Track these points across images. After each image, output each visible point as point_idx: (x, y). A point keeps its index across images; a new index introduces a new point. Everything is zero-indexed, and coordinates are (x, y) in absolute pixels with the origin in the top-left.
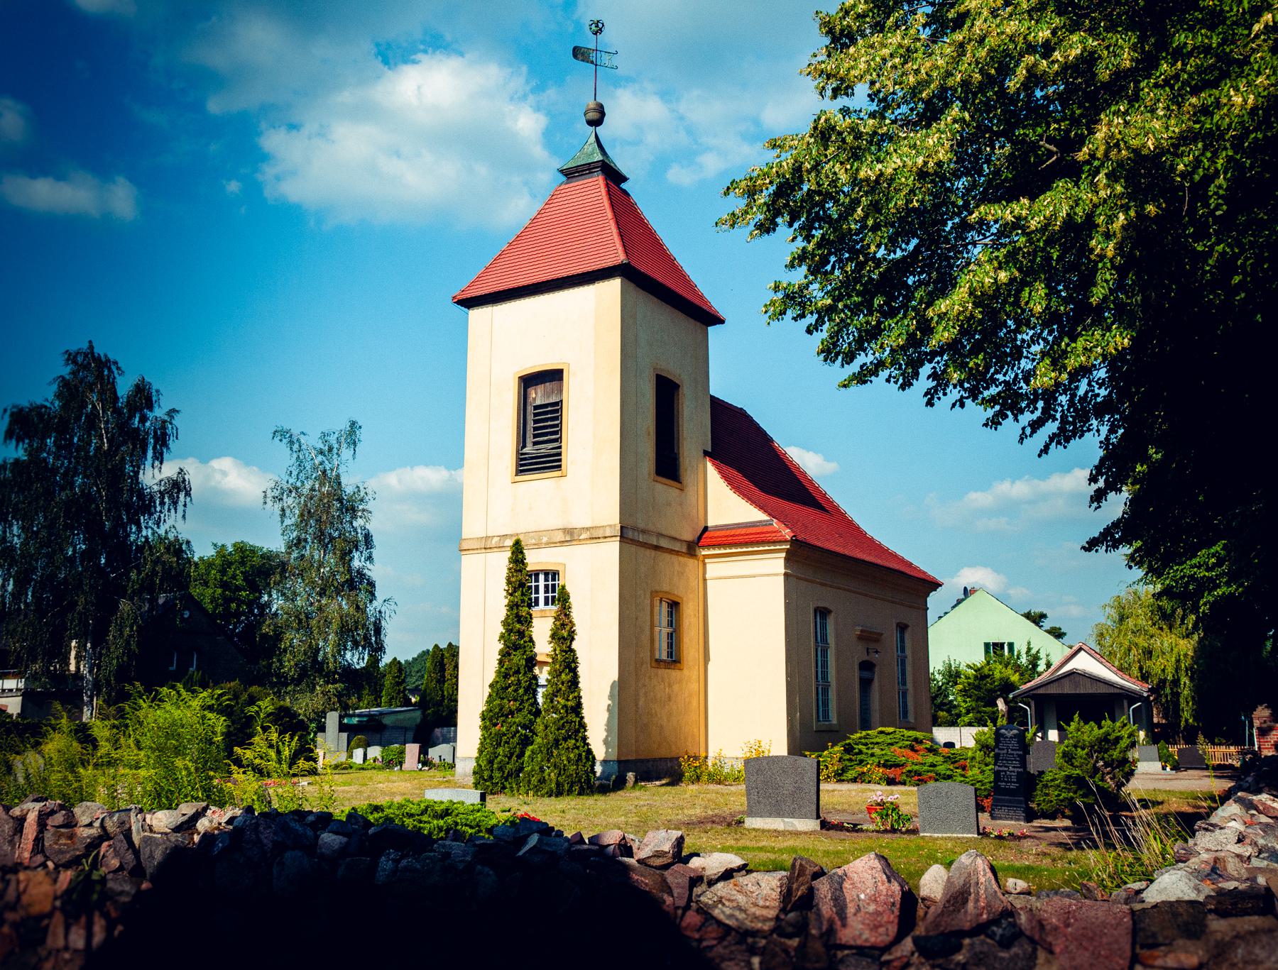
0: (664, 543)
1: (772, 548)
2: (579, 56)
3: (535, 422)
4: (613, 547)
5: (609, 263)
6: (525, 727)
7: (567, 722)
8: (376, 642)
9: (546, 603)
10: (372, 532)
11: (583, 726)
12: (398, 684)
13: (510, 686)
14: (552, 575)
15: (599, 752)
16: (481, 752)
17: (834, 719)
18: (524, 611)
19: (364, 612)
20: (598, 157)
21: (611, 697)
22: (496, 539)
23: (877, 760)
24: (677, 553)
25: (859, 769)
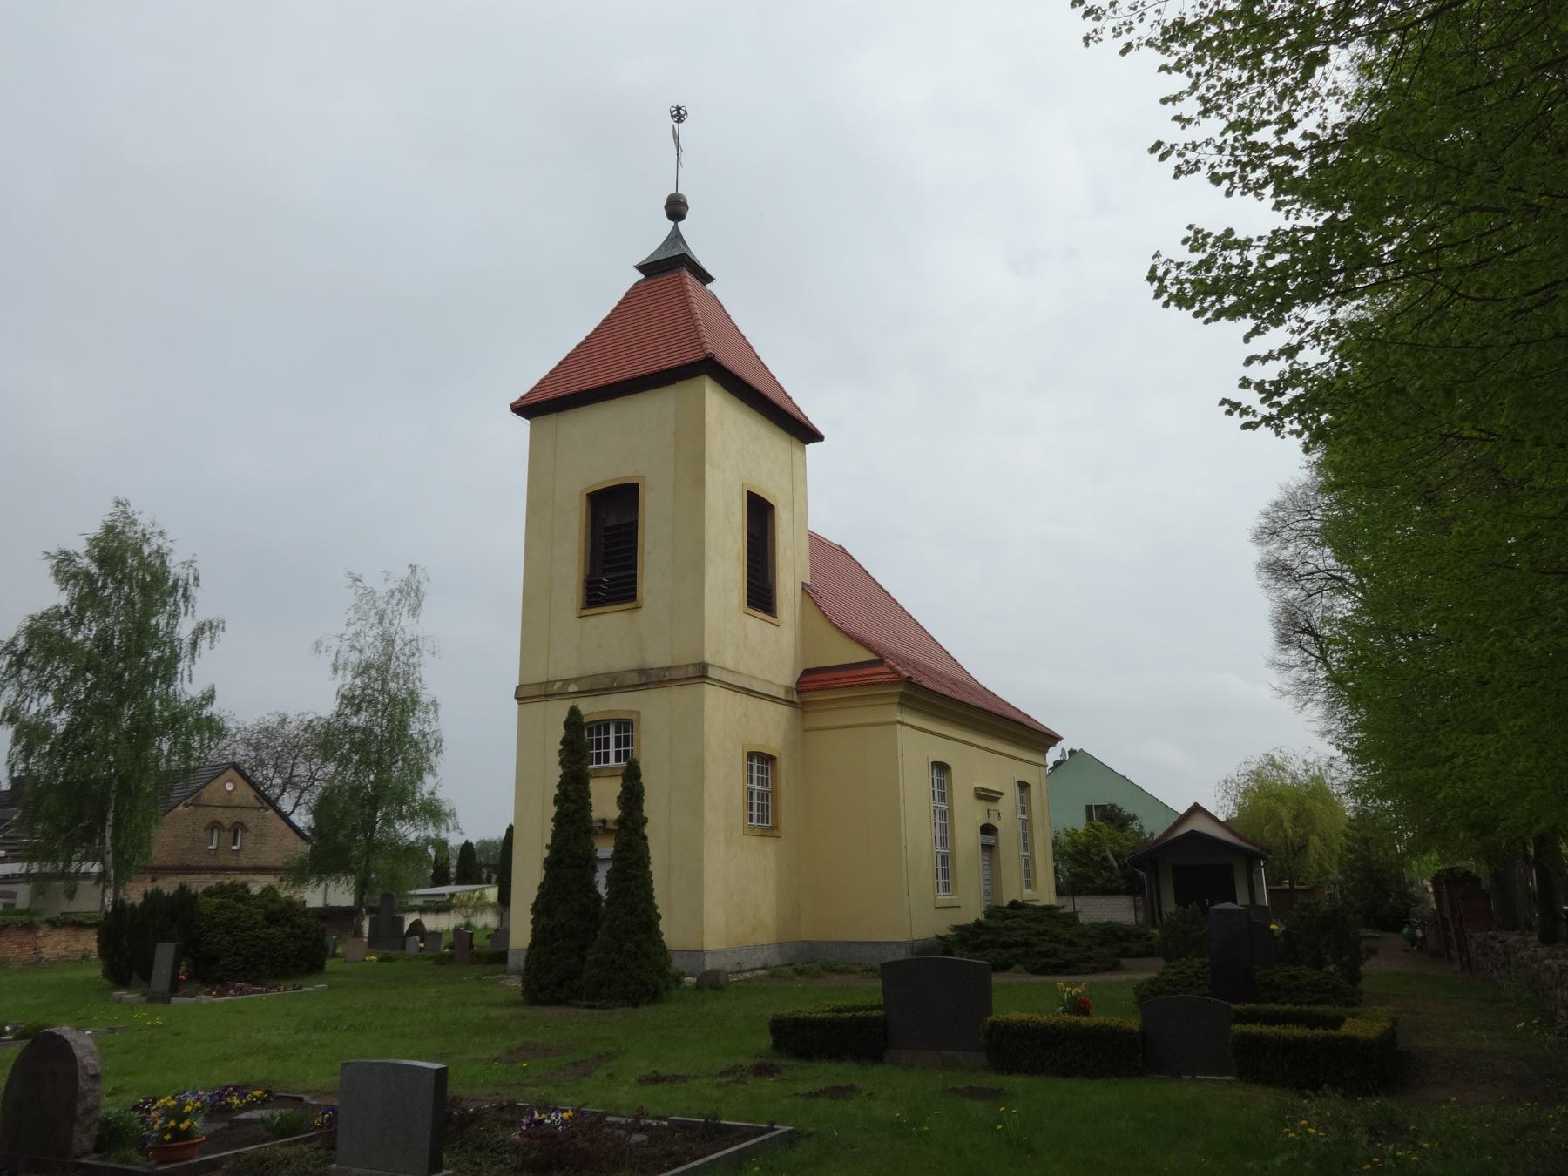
9: (618, 759)
22: (557, 685)
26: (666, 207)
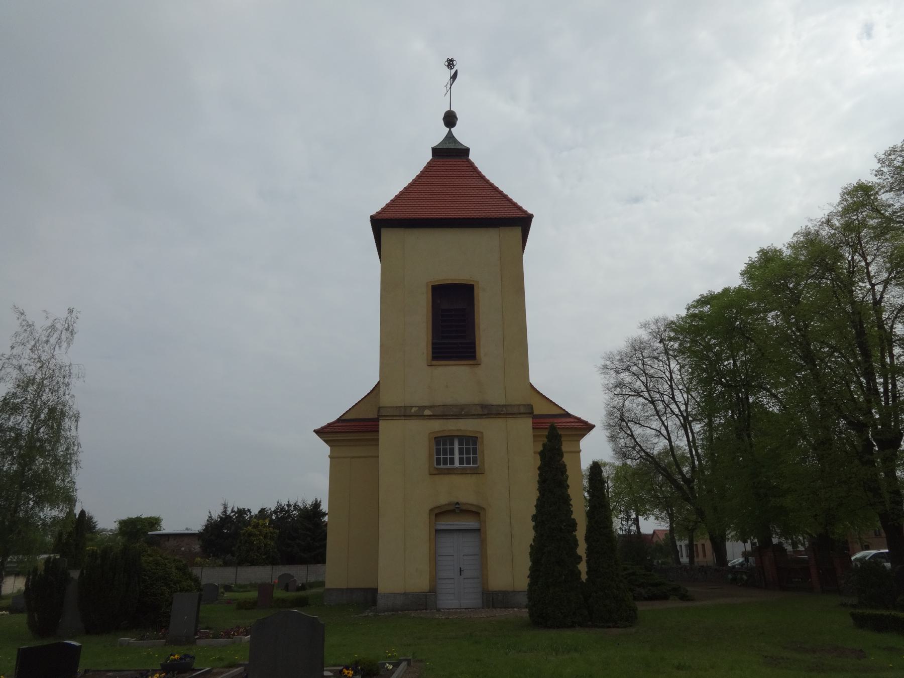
26: (444, 119)
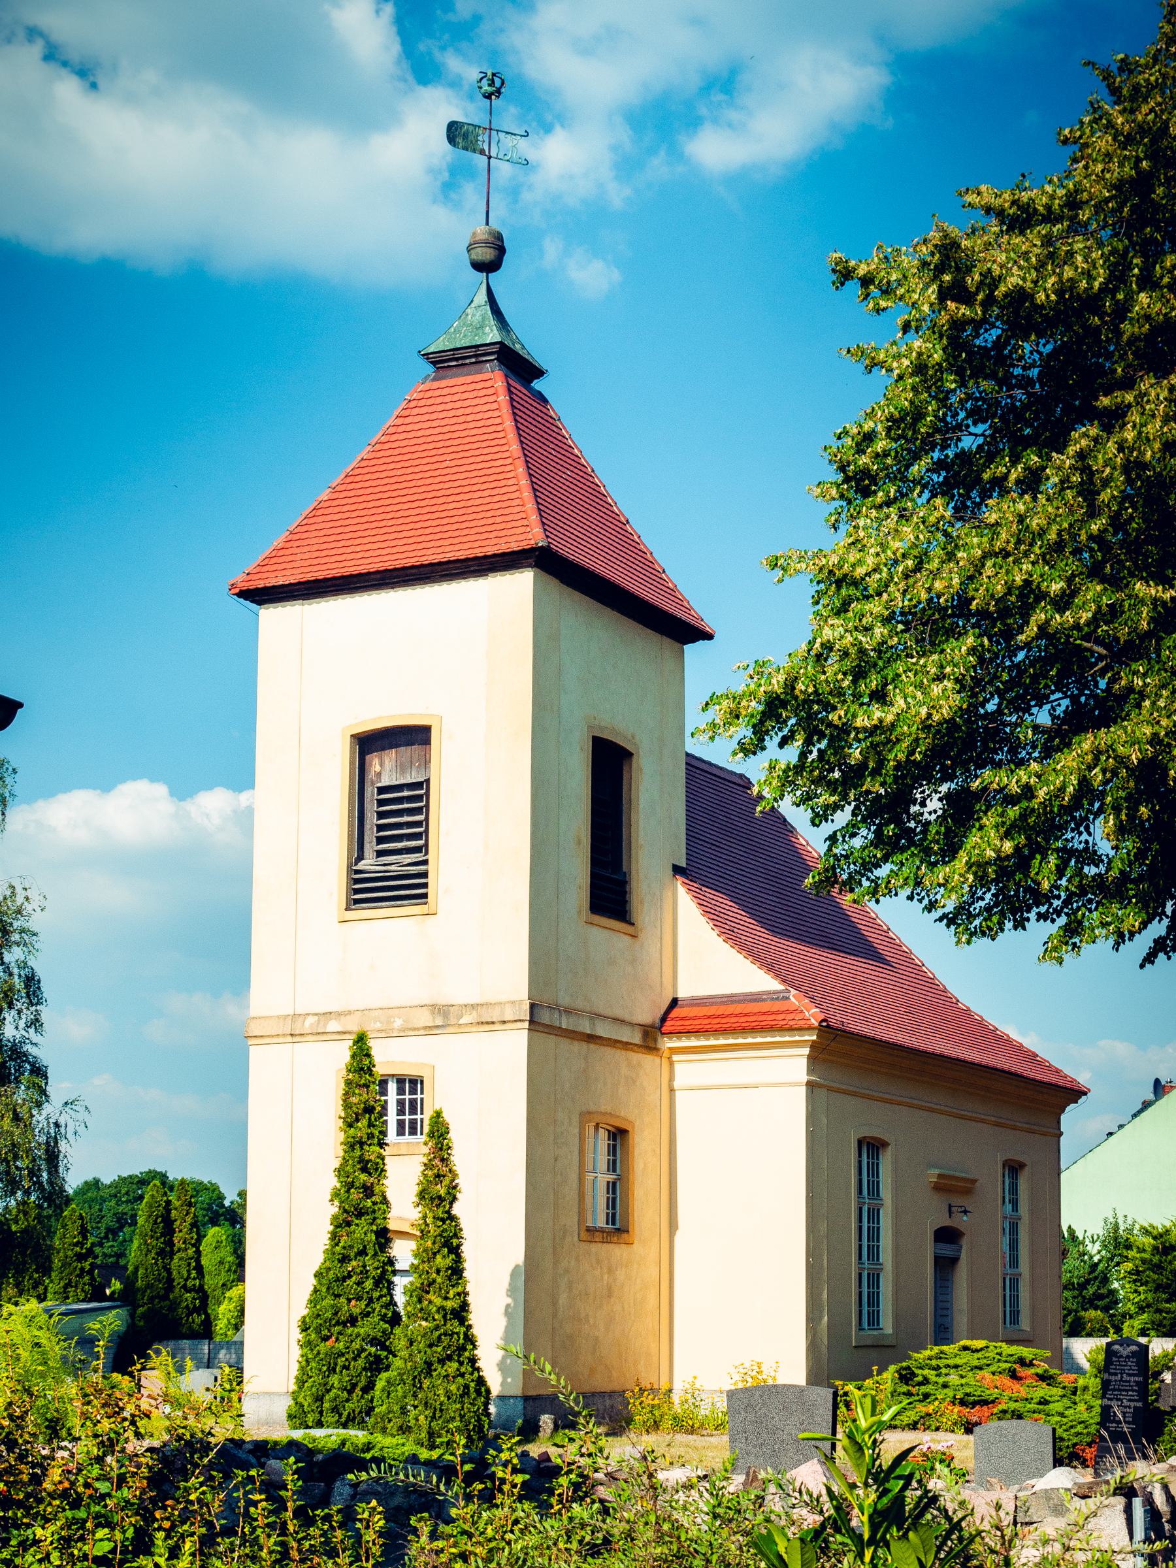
0: (602, 1030)
1: (787, 1039)
2: (459, 140)
3: (381, 815)
4: (518, 1040)
5: (514, 544)
6: (374, 1342)
7: (445, 1334)
8: (50, 1182)
9: (401, 1132)
10: (40, 972)
11: (470, 1340)
12: (81, 1257)
13: (349, 1276)
14: (411, 1083)
15: (495, 1383)
16: (301, 1383)
17: (887, 1324)
18: (372, 1152)
19: (28, 1126)
20: (492, 335)
21: (511, 1292)
22: (311, 1020)
23: (951, 1394)
24: (626, 1046)
25: (922, 1408)
